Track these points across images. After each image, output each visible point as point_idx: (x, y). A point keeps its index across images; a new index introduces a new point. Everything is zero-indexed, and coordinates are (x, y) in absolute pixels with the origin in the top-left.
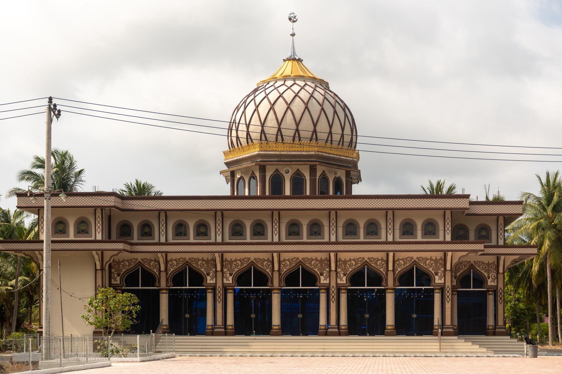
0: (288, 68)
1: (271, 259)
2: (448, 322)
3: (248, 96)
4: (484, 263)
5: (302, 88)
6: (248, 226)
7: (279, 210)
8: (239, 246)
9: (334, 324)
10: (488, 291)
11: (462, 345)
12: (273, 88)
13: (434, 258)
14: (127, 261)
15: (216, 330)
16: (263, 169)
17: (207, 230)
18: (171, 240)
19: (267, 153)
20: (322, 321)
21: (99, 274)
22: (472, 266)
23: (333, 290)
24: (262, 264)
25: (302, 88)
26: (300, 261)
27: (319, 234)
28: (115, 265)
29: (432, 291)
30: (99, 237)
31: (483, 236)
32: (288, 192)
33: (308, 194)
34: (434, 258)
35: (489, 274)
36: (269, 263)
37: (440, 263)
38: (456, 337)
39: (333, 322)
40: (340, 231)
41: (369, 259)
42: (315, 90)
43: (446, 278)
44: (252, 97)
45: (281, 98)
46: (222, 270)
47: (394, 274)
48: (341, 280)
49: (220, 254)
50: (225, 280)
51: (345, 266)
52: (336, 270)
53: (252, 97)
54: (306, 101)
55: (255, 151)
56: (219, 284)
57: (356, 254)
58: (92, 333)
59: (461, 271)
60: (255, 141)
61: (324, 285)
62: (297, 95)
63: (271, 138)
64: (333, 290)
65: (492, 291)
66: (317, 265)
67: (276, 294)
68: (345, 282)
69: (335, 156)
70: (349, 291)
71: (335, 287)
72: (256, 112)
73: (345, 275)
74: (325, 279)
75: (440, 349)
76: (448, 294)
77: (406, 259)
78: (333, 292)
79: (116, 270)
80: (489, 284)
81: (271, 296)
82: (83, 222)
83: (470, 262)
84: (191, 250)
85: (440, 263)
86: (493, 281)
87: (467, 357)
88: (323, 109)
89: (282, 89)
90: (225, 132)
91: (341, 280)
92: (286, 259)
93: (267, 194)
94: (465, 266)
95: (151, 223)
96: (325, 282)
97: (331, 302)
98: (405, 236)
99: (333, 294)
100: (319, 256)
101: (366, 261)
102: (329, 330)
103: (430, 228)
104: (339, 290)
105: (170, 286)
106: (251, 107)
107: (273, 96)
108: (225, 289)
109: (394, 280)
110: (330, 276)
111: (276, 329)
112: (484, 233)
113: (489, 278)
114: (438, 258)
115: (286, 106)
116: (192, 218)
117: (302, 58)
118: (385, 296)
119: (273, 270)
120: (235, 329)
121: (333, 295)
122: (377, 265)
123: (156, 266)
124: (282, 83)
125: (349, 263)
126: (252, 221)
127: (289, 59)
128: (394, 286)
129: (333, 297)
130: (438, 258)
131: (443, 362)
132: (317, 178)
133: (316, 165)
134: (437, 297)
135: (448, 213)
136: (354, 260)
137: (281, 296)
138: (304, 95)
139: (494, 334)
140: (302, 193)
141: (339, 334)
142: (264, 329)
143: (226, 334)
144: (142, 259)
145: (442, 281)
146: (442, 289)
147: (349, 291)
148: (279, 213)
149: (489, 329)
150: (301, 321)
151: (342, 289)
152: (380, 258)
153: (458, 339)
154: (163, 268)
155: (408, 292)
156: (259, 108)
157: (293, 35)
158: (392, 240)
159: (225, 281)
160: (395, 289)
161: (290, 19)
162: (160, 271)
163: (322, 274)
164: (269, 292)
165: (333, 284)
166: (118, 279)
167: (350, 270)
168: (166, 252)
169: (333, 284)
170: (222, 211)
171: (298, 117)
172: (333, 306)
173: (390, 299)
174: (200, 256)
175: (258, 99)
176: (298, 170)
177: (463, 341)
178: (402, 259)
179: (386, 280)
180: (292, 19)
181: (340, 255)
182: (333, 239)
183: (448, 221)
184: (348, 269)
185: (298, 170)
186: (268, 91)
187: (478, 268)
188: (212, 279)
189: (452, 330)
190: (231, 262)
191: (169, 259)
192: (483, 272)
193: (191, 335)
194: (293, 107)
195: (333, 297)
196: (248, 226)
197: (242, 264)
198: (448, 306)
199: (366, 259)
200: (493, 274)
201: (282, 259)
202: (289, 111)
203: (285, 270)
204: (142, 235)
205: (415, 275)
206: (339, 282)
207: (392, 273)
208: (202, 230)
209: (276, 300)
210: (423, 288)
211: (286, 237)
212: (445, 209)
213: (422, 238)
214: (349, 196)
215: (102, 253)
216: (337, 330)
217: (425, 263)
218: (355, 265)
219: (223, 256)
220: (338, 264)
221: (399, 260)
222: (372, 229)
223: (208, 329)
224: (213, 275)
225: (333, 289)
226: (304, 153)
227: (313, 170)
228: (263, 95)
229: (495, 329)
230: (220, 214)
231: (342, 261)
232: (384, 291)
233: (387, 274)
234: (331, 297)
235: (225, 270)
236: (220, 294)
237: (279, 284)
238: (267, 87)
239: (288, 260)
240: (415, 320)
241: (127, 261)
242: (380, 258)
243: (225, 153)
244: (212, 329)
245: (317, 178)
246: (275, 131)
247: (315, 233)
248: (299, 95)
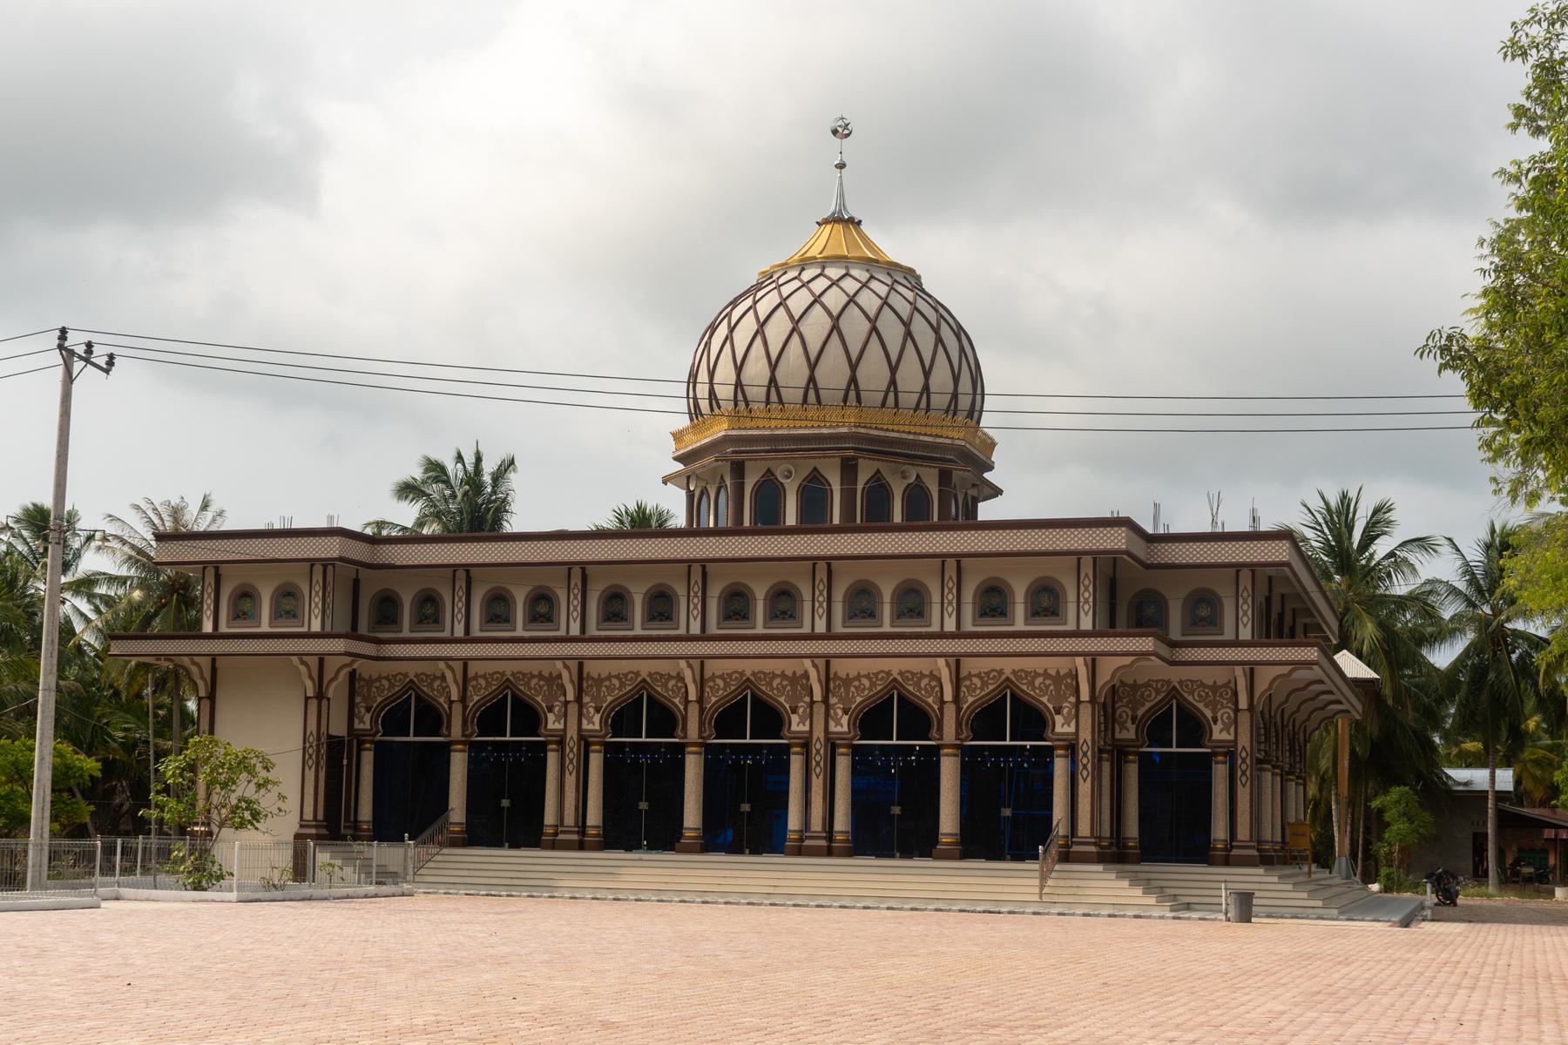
0: (820, 241)
2: (1084, 829)
3: (734, 303)
4: (1203, 685)
5: (865, 285)
6: (760, 592)
7: (958, 557)
8: (626, 645)
9: (819, 828)
10: (1215, 754)
11: (1105, 886)
12: (797, 284)
13: (1053, 672)
14: (617, 677)
15: (807, 842)
16: (738, 469)
17: (551, 607)
18: (476, 632)
19: (743, 433)
20: (1219, 831)
21: (313, 705)
22: (1173, 693)
23: (818, 746)
24: (665, 686)
25: (865, 285)
27: (792, 617)
29: (786, 749)
30: (1087, 624)
31: (1202, 619)
32: (791, 519)
33: (836, 521)
34: (1053, 672)
35: (1214, 711)
37: (1067, 685)
38: (1100, 868)
39: (1243, 833)
40: (968, 611)
41: (901, 673)
42: (892, 288)
43: (1082, 720)
44: (749, 302)
45: (782, 309)
46: (825, 700)
47: (958, 710)
49: (1089, 659)
50: (585, 722)
53: (749, 302)
54: (872, 314)
55: (720, 430)
56: (572, 732)
57: (874, 661)
58: (292, 839)
59: (1148, 705)
60: (754, 406)
61: (553, 733)
62: (852, 300)
63: (792, 395)
64: (818, 746)
65: (1225, 755)
66: (1047, 687)
69: (904, 436)
70: (856, 750)
72: (759, 340)
73: (845, 712)
74: (802, 722)
75: (1041, 895)
76: (1085, 761)
77: (988, 674)
79: (365, 699)
80: (1217, 735)
81: (938, 762)
82: (289, 594)
83: (1169, 682)
84: (514, 654)
85: (1067, 685)
86: (1226, 728)
87: (1136, 917)
88: (874, 329)
89: (819, 286)
90: (682, 389)
91: (590, 721)
92: (481, 673)
93: (747, 523)
94: (1158, 691)
95: (670, 588)
98: (239, 621)
99: (818, 758)
100: (1053, 665)
102: (1235, 852)
103: (1046, 600)
106: (748, 327)
107: (798, 303)
108: (832, 745)
109: (959, 725)
112: (1204, 612)
113: (1215, 722)
114: (1062, 672)
115: (790, 326)
116: (613, 578)
117: (857, 217)
120: (604, 835)
122: (920, 689)
123: (933, 688)
124: (818, 271)
126: (528, 589)
127: (826, 222)
130: (1062, 672)
131: (1048, 929)
132: (860, 487)
133: (855, 459)
134: (1060, 766)
135: (1087, 562)
136: (867, 676)
137: (706, 760)
138: (869, 301)
139: (1227, 862)
140: (776, 522)
141: (829, 852)
142: (661, 834)
143: (581, 846)
144: (650, 675)
145: (1072, 729)
146: (1072, 748)
147: (856, 750)
148: (829, 565)
149: (1215, 849)
150: (747, 819)
153: (1105, 871)
154: (693, 696)
155: (990, 756)
156: (735, 334)
157: (841, 166)
158: (953, 629)
159: (585, 725)
161: (835, 132)
162: (687, 702)
163: (794, 710)
164: (680, 749)
166: (597, 718)
167: (859, 699)
168: (459, 658)
169: (819, 733)
170: (467, 568)
171: (814, 350)
172: (1243, 795)
173: (949, 769)
174: (534, 667)
175: (763, 308)
176: (815, 469)
177: (1113, 876)
178: (979, 676)
179: (940, 722)
180: (841, 132)
181: (592, 668)
182: (950, 626)
183: (1087, 582)
185: (815, 469)
186: (786, 290)
187: (1190, 698)
188: (557, 720)
189: (1093, 849)
190: (847, 681)
191: (471, 673)
192: (1201, 706)
193: (511, 847)
194: (844, 324)
196: (760, 592)
197: (622, 685)
198: (1085, 788)
199: (895, 674)
200: (1225, 713)
201: (707, 674)
202: (795, 337)
203: (714, 699)
204: (491, 620)
205: (1011, 713)
208: (543, 608)
209: (949, 769)
210: (1028, 744)
211: (974, 620)
212: (1079, 554)
213: (1026, 623)
214: (970, 521)
215: (958, 662)
216: (823, 843)
217: (1031, 683)
218: (870, 689)
219: (580, 668)
221: (970, 676)
222: (542, 608)
226: (825, 431)
227: (849, 470)
228: (773, 299)
230: (583, 572)
232: (935, 751)
235: (833, 700)
236: (818, 758)
237: (700, 732)
238: (781, 281)
239: (721, 677)
240: (1007, 823)
241: (387, 678)
243: (678, 436)
244: (1225, 849)
245: (860, 487)
246: (802, 380)
247: (784, 613)
248: (823, 299)
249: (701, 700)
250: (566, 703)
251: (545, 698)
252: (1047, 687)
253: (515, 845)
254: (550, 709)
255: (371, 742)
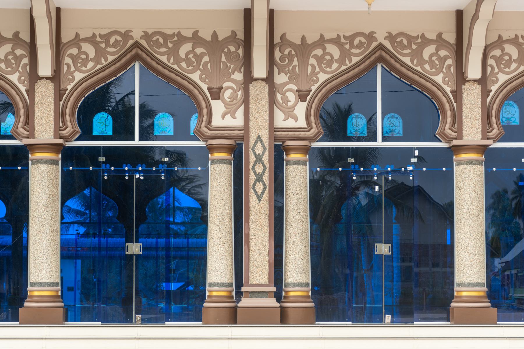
1: (25, 36)
14: (336, 41)
26: (137, 45)
28: (290, 57)
36: (19, 52)
37: (229, 55)
39: (259, 271)
48: (290, 114)
51: (304, 63)
52: (269, 80)
67: (43, 168)
68: (302, 123)
71: (266, 139)
73: (302, 96)
78: (259, 159)
81: (26, 173)
91: (290, 114)
96: (229, 121)
97: (253, 197)
101: (381, 47)
102: (245, 302)
104: (279, 152)
105: (66, 138)
110: (246, 101)
111: (42, 299)
118: (450, 173)
119: (34, 77)
121: (259, 169)
125: (319, 52)
128: (57, 135)
129: (259, 178)
151: (288, 150)
152: (432, 36)
160: (483, 149)
165: (259, 129)
166: (301, 109)
167: (323, 77)
169: (259, 129)
179: (457, 118)
184: (72, 74)
195: (259, 178)
203: (78, 76)
206: (281, 121)
207: (477, 89)
216: (272, 302)
220: (278, 55)
223: (461, 300)
224: (233, 97)
225: (259, 149)
229: (239, 294)
231: (291, 44)
233: (457, 94)
234: (252, 178)
235: (280, 78)
241: (336, 41)
242: (432, 36)
249: (56, 77)
250: (483, 81)
251: (206, 76)
252: (198, 58)
253: (155, 318)
254: (216, 93)
255: (306, 150)
